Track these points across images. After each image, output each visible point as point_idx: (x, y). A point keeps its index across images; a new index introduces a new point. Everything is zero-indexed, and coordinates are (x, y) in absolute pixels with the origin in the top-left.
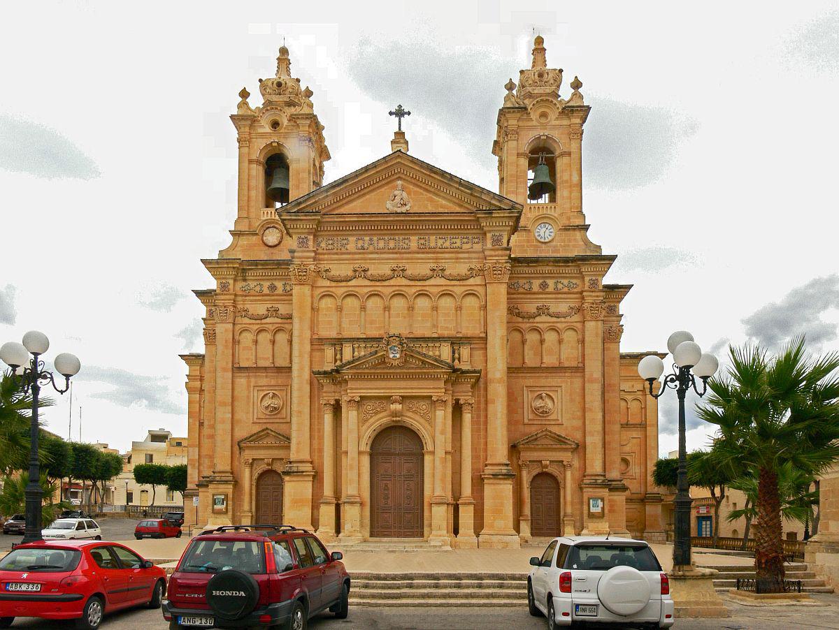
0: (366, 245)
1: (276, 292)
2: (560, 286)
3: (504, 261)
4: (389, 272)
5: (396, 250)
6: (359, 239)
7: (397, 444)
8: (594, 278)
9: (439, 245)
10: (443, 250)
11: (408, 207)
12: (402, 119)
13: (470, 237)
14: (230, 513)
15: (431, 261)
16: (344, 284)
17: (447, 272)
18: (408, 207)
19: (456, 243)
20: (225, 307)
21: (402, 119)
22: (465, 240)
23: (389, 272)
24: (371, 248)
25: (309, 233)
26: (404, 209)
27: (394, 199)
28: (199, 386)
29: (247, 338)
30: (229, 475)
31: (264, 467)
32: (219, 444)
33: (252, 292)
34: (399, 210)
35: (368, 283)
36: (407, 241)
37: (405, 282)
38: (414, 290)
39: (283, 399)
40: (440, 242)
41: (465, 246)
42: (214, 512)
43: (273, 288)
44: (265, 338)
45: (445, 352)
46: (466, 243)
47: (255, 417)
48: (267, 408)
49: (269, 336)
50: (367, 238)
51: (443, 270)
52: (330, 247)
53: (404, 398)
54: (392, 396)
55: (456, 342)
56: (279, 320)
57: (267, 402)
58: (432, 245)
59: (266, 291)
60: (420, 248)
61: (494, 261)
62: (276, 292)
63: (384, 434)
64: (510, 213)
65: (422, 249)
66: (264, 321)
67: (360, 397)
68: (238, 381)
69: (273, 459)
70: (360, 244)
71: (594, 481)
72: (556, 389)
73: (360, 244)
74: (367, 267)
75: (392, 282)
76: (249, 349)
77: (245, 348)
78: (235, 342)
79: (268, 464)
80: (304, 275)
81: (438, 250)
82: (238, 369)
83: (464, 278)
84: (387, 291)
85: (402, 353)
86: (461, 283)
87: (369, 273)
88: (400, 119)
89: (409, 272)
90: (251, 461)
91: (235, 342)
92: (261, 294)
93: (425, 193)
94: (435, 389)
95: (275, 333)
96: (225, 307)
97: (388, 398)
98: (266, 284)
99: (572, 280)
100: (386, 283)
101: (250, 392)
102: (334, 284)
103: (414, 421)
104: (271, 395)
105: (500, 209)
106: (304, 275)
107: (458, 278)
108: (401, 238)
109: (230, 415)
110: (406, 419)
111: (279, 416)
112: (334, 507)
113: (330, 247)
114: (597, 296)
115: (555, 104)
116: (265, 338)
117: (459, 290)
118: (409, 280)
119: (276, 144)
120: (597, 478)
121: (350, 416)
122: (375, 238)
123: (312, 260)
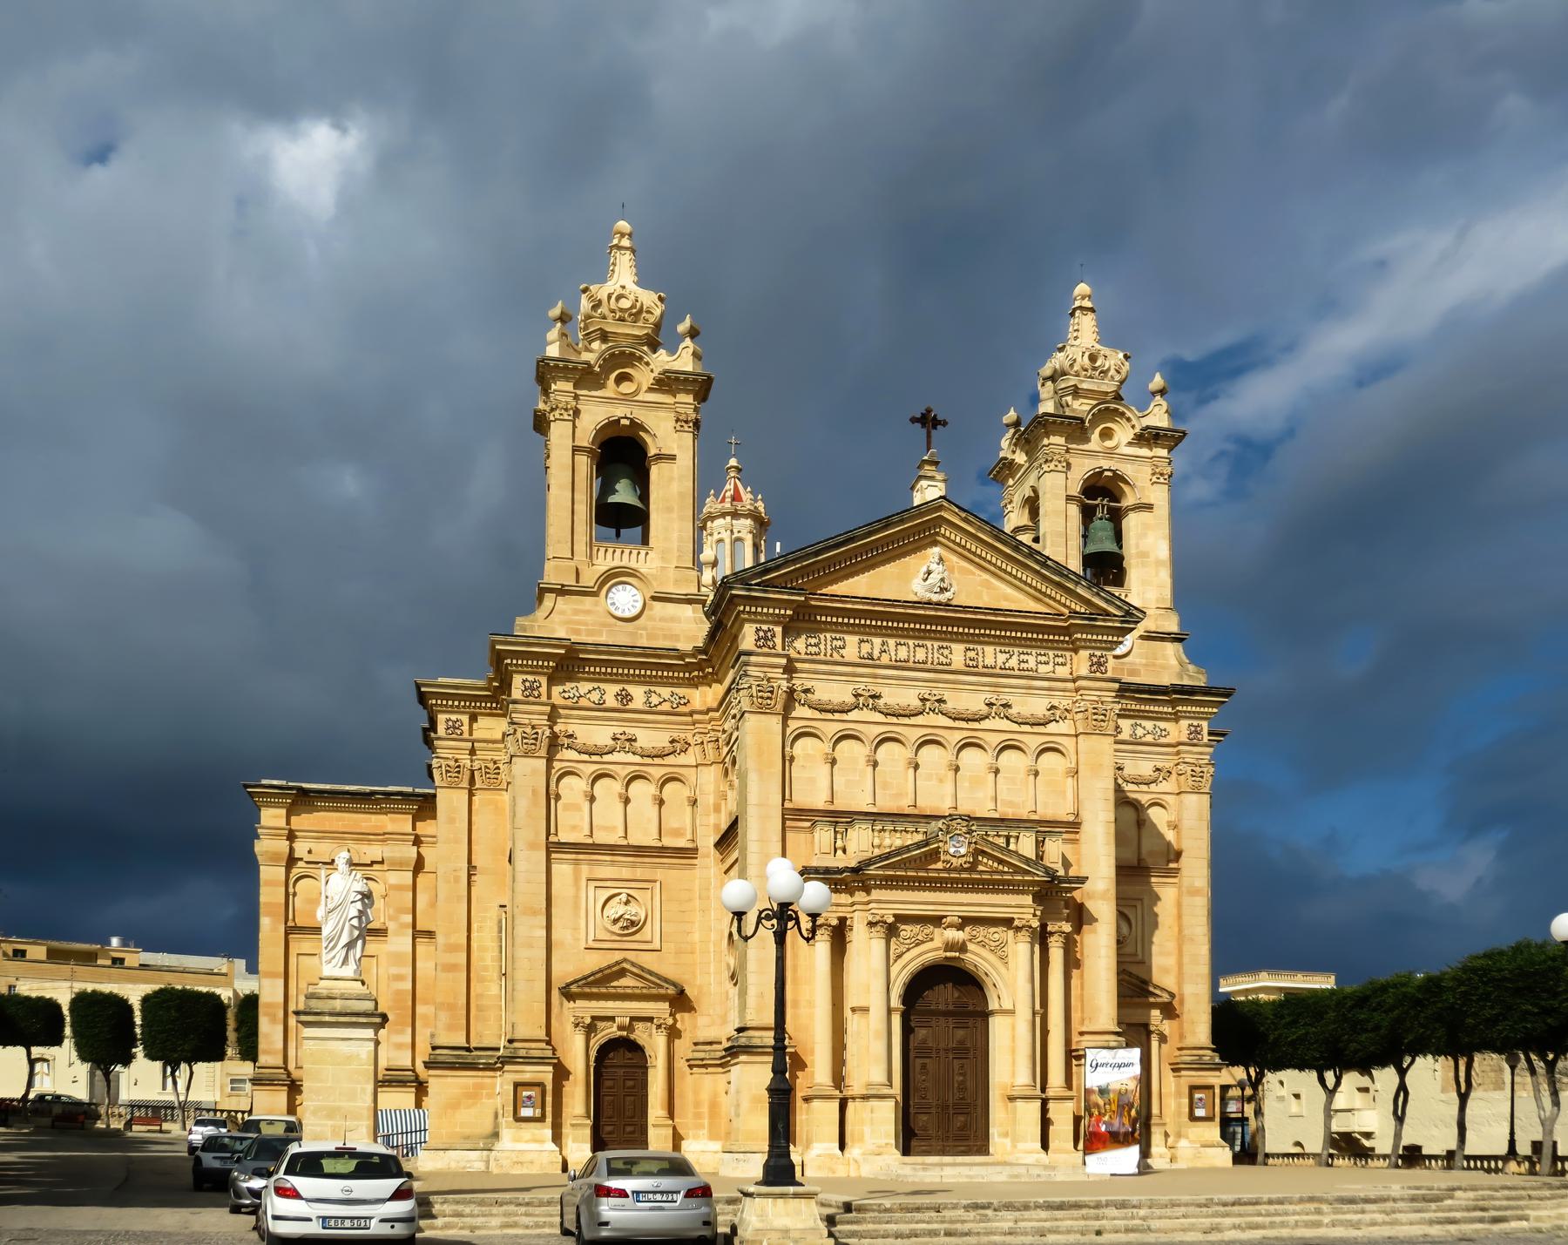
0: (876, 654)
1: (631, 706)
2: (1140, 732)
3: (1110, 699)
4: (917, 703)
5: (929, 666)
6: (863, 641)
7: (944, 996)
8: (1195, 723)
9: (1000, 663)
10: (1006, 672)
11: (948, 595)
12: (934, 432)
13: (1051, 653)
14: (549, 1119)
15: (987, 688)
16: (837, 716)
17: (1013, 711)
18: (948, 595)
19: (1027, 662)
20: (533, 727)
21: (934, 432)
22: (1043, 659)
23: (917, 703)
24: (885, 659)
25: (776, 623)
26: (943, 598)
27: (927, 579)
28: (287, 850)
29: (573, 789)
30: (543, 1045)
31: (610, 1031)
32: (520, 986)
33: (583, 702)
34: (935, 598)
35: (879, 717)
36: (946, 652)
37: (944, 721)
38: (958, 735)
39: (645, 904)
40: (1002, 658)
41: (1043, 669)
42: (1193, 1118)
43: (625, 697)
44: (642, 792)
45: (1026, 845)
46: (1062, 664)
47: (591, 937)
48: (615, 921)
49: (617, 787)
50: (877, 641)
51: (1007, 706)
52: (814, 650)
53: (966, 922)
54: (945, 917)
55: (1044, 828)
56: (637, 759)
57: (615, 909)
58: (989, 661)
59: (611, 702)
60: (969, 666)
61: (1097, 699)
62: (631, 706)
63: (922, 983)
64: (1123, 622)
65: (971, 669)
66: (607, 758)
67: (895, 916)
68: (556, 868)
69: (633, 1019)
70: (866, 648)
71: (1197, 1058)
72: (1133, 903)
73: (866, 648)
74: (877, 690)
75: (919, 720)
76: (577, 808)
77: (567, 807)
78: (551, 797)
79: (621, 1028)
80: (768, 698)
81: (998, 671)
82: (554, 848)
83: (1042, 721)
84: (913, 735)
85: (969, 846)
86: (1037, 729)
87: (881, 702)
88: (929, 436)
89: (949, 706)
90: (588, 1021)
91: (551, 797)
92: (600, 707)
93: (978, 572)
94: (1022, 907)
95: (663, 785)
96: (533, 727)
97: (937, 921)
98: (612, 689)
99: (1158, 723)
100: (913, 720)
101: (578, 889)
102: (817, 715)
103: (979, 958)
104: (624, 897)
105: (1108, 614)
106: (768, 698)
107: (1032, 721)
108: (936, 646)
109: (544, 933)
110: (968, 957)
111: (637, 937)
112: (837, 1104)
113: (814, 650)
114: (1201, 753)
115: (1129, 420)
116: (642, 792)
117: (1033, 742)
118: (950, 717)
119: (626, 422)
120: (1201, 1052)
121: (866, 949)
122: (892, 642)
123: (781, 670)
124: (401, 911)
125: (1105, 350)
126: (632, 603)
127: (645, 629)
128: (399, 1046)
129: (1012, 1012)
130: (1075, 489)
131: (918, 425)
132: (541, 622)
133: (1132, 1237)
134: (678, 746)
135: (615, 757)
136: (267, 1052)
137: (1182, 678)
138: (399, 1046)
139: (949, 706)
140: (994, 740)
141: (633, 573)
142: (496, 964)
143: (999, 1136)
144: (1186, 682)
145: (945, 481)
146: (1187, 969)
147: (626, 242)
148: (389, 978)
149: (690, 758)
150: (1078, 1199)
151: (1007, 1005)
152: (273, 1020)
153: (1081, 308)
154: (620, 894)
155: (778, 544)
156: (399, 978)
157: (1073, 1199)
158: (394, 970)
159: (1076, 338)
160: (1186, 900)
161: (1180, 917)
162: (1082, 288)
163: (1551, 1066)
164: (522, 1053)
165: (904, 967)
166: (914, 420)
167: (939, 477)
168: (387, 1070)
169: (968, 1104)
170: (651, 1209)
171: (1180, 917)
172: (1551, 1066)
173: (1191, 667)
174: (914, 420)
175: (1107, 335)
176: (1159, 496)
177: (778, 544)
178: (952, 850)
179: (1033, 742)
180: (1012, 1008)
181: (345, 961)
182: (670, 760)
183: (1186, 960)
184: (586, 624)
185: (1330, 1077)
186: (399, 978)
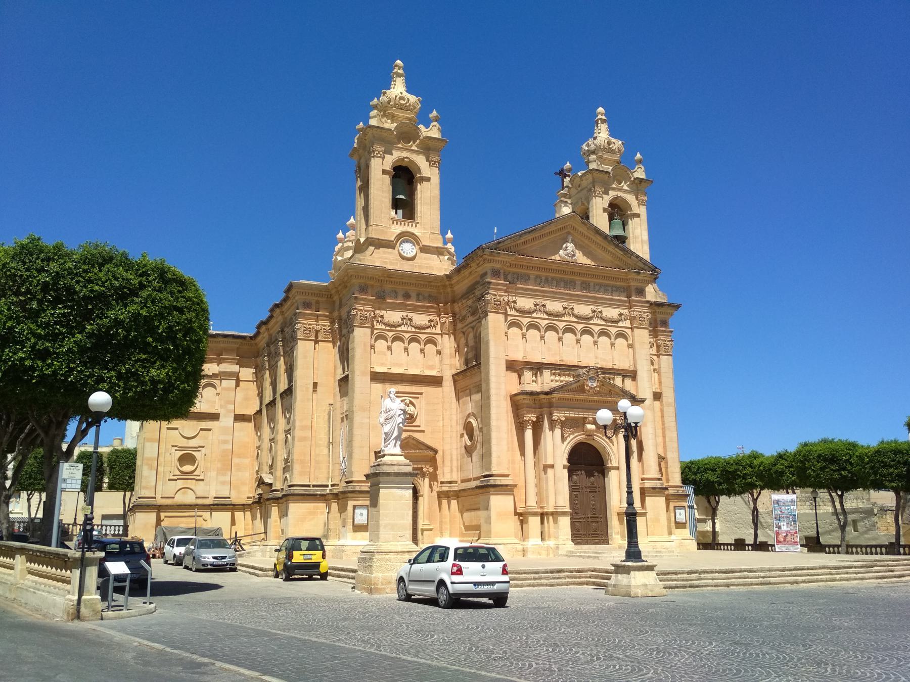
4: (561, 310)
84: (561, 325)
124: (228, 402)
125: (613, 140)
126: (410, 251)
127: (418, 263)
128: (223, 483)
129: (617, 468)
130: (606, 206)
131: (558, 176)
132: (368, 257)
133: (765, 587)
134: (433, 323)
135: (403, 328)
136: (146, 488)
137: (657, 298)
138: (223, 483)
139: (604, 314)
140: (596, 329)
141: (412, 235)
142: (326, 437)
143: (615, 534)
144: (659, 300)
145: (571, 204)
146: (668, 444)
147: (401, 71)
148: (219, 443)
149: (438, 330)
150: (732, 568)
151: (615, 464)
152: (151, 468)
153: (601, 119)
154: (405, 400)
155: (496, 228)
156: (225, 442)
157: (731, 568)
158: (222, 438)
159: (599, 133)
160: (666, 409)
161: (663, 417)
162: (601, 110)
163: (841, 497)
164: (357, 489)
165: (569, 443)
166: (556, 173)
167: (569, 201)
168: (215, 498)
169: (597, 517)
170: (877, 578)
171: (663, 417)
172: (841, 497)
173: (660, 292)
174: (556, 173)
175: (612, 133)
176: (642, 211)
177: (496, 228)
178: (590, 384)
179: (613, 331)
180: (617, 465)
181: (395, 446)
182: (428, 331)
183: (667, 440)
184: (390, 259)
185: (712, 499)
186: (225, 442)
